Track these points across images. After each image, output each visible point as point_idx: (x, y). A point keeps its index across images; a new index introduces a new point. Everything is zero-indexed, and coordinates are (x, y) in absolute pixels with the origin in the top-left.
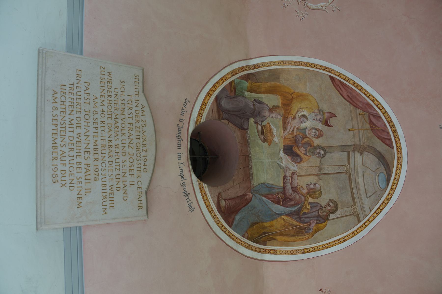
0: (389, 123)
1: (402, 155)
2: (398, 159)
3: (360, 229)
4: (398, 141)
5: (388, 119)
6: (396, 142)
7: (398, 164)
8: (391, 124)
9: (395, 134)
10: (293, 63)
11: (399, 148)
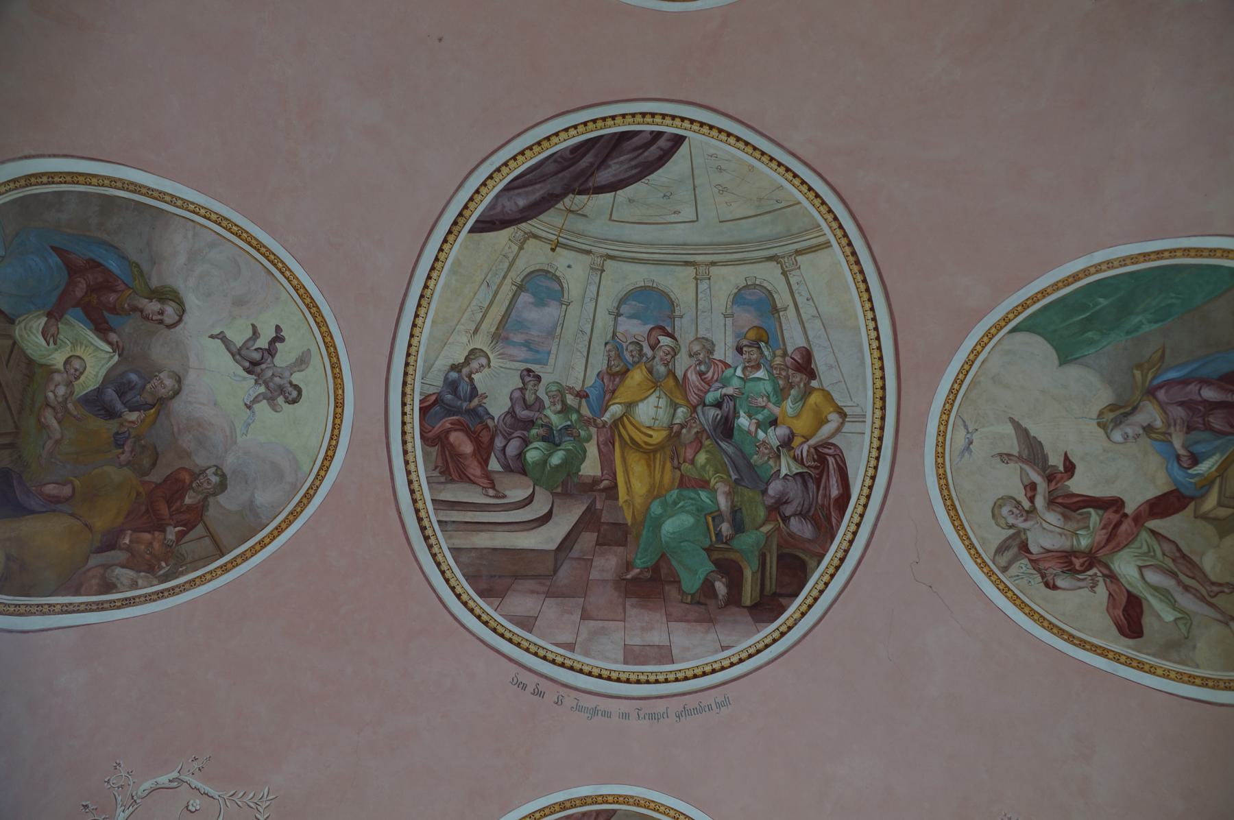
0: (565, 809)
1: (632, 797)
2: (638, 805)
3: (941, 471)
4: (604, 799)
5: (557, 808)
6: (603, 803)
7: (648, 808)
8: (568, 805)
9: (589, 801)
10: (1036, 617)
11: (617, 799)
